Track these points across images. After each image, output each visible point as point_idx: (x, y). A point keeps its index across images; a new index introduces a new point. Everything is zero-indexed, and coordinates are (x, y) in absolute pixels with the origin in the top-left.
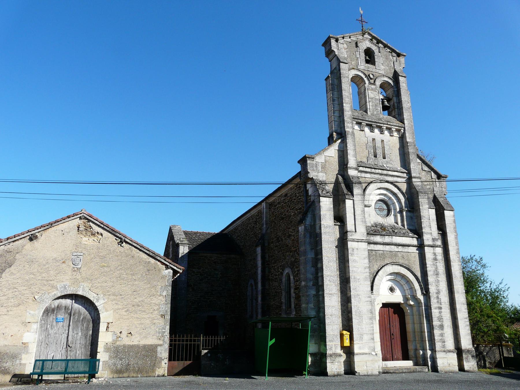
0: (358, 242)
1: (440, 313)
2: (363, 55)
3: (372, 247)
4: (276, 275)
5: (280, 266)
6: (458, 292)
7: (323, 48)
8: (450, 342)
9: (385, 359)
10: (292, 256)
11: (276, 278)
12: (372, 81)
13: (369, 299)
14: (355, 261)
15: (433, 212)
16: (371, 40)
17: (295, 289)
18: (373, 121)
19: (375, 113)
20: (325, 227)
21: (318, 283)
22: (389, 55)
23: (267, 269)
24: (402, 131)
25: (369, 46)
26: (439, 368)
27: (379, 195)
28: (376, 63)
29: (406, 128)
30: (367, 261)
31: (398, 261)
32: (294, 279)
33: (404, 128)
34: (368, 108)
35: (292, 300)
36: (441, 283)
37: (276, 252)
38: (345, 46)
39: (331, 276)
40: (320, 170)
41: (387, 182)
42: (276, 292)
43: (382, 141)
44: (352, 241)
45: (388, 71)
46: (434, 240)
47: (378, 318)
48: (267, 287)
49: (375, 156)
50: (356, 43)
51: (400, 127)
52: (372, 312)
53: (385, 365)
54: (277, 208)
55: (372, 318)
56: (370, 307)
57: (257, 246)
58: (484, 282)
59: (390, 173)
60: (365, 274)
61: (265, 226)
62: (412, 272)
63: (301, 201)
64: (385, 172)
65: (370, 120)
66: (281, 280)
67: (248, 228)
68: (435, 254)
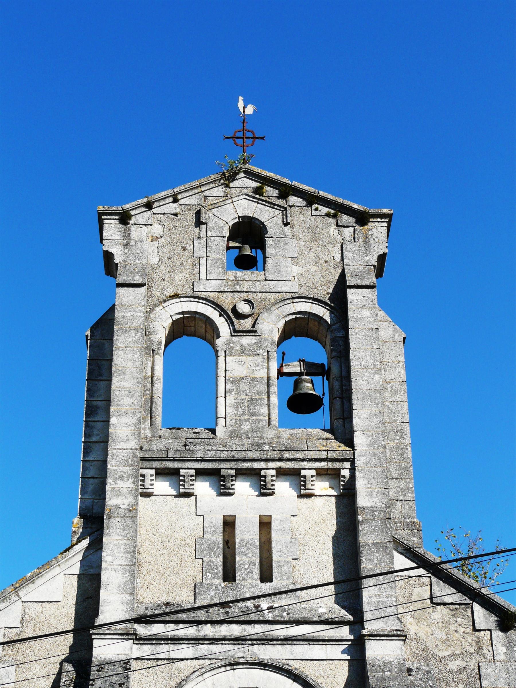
12: (247, 324)
16: (258, 191)
18: (224, 455)
19: (246, 426)
22: (327, 225)
24: (346, 473)
29: (359, 463)
33: (353, 462)
34: (221, 413)
38: (157, 229)
43: (265, 524)
45: (318, 278)
50: (198, 214)
51: (333, 460)
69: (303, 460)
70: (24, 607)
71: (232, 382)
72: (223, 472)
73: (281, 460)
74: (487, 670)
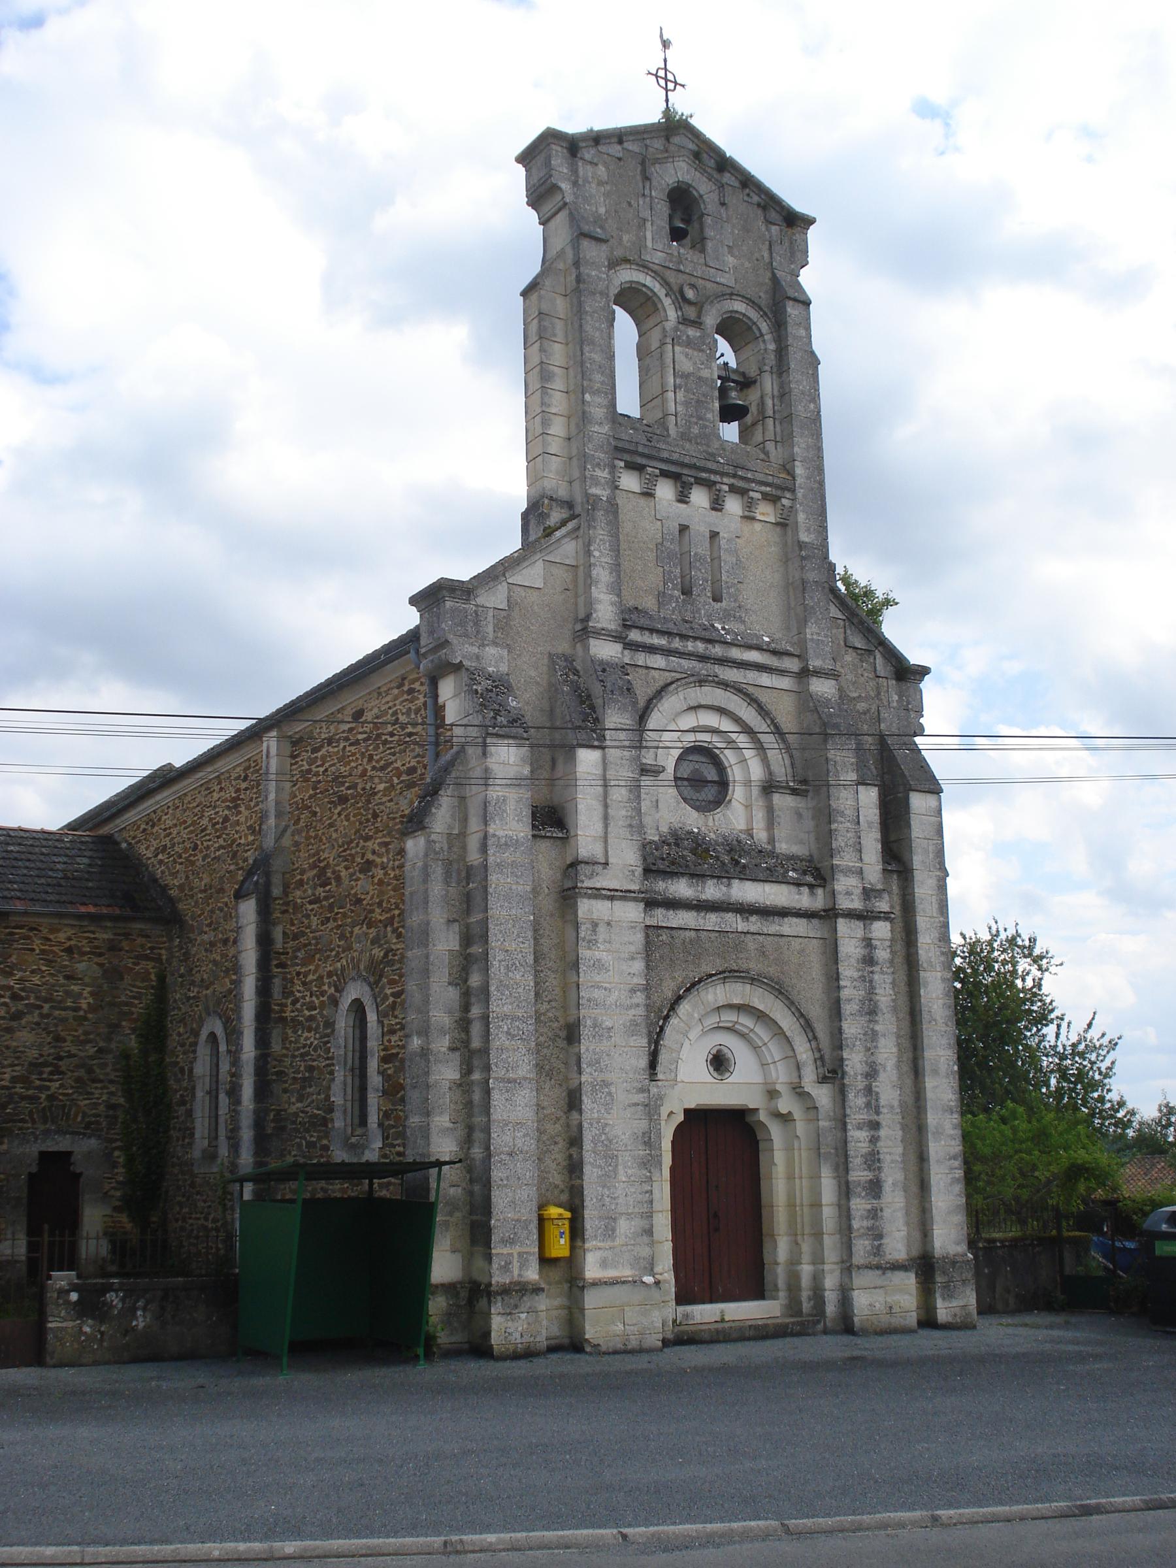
0: (611, 898)
1: (874, 1140)
2: (663, 208)
3: (661, 917)
4: (312, 1007)
5: (330, 975)
6: (935, 1072)
7: (521, 171)
8: (897, 1234)
9: (683, 1298)
10: (375, 941)
11: (311, 1018)
13: (640, 1098)
14: (598, 965)
15: (869, 797)
17: (385, 1060)
18: (687, 460)
19: (695, 430)
20: (499, 846)
21: (466, 1043)
23: (277, 982)
25: (687, 178)
26: (856, 1319)
27: (693, 730)
28: (709, 245)
30: (639, 966)
31: (744, 967)
32: (380, 1022)
35: (373, 1100)
36: (882, 1042)
37: (315, 921)
38: (601, 170)
39: (514, 1018)
40: (491, 636)
41: (725, 685)
42: (311, 1069)
43: (714, 535)
44: (590, 897)
46: (868, 893)
47: (667, 1160)
48: (276, 1047)
49: (687, 592)
52: (649, 1140)
53: (686, 1316)
54: (323, 758)
55: (650, 1162)
56: (643, 1125)
57: (239, 896)
58: (1043, 1018)
59: (736, 653)
60: (632, 1012)
61: (272, 821)
62: (791, 1004)
63: (416, 743)
64: (717, 650)
65: (675, 457)
66: (330, 1024)
67: (205, 822)
68: (868, 943)
69: (753, 481)
70: (509, 590)
71: (681, 377)
72: (684, 478)
73: (735, 476)
74: (884, 714)
